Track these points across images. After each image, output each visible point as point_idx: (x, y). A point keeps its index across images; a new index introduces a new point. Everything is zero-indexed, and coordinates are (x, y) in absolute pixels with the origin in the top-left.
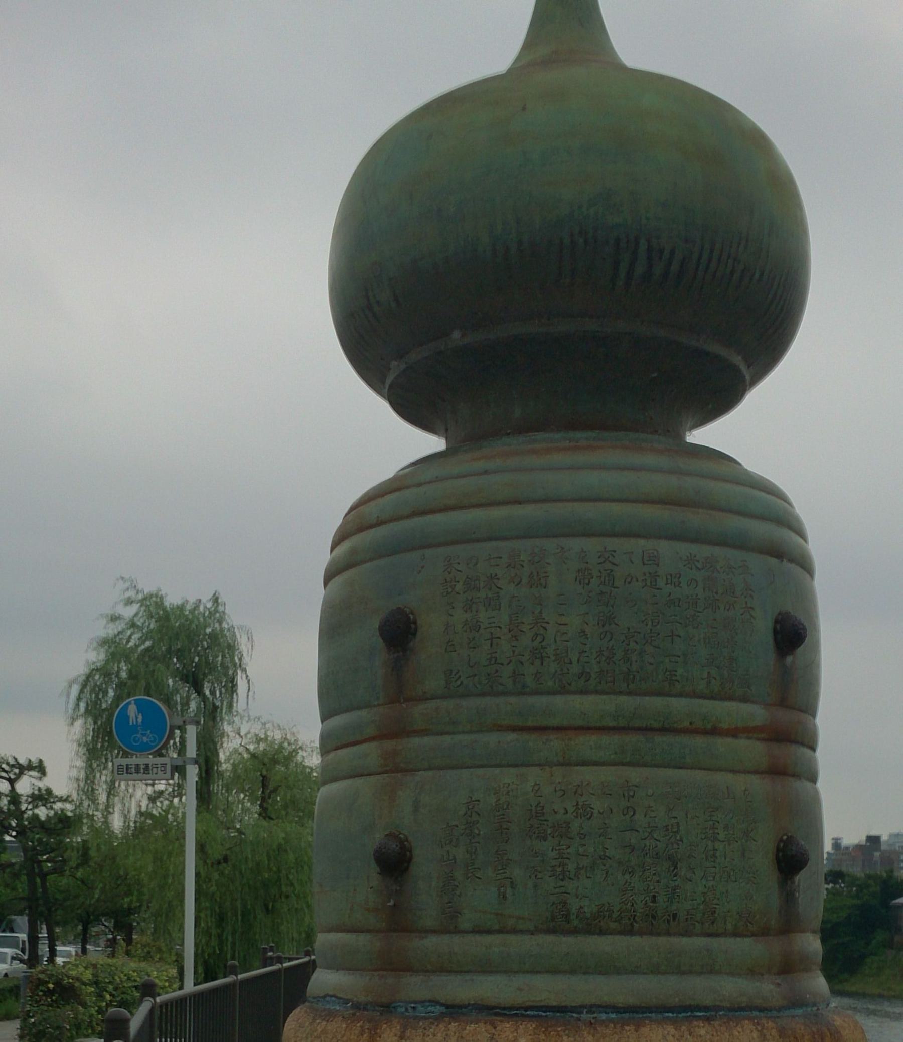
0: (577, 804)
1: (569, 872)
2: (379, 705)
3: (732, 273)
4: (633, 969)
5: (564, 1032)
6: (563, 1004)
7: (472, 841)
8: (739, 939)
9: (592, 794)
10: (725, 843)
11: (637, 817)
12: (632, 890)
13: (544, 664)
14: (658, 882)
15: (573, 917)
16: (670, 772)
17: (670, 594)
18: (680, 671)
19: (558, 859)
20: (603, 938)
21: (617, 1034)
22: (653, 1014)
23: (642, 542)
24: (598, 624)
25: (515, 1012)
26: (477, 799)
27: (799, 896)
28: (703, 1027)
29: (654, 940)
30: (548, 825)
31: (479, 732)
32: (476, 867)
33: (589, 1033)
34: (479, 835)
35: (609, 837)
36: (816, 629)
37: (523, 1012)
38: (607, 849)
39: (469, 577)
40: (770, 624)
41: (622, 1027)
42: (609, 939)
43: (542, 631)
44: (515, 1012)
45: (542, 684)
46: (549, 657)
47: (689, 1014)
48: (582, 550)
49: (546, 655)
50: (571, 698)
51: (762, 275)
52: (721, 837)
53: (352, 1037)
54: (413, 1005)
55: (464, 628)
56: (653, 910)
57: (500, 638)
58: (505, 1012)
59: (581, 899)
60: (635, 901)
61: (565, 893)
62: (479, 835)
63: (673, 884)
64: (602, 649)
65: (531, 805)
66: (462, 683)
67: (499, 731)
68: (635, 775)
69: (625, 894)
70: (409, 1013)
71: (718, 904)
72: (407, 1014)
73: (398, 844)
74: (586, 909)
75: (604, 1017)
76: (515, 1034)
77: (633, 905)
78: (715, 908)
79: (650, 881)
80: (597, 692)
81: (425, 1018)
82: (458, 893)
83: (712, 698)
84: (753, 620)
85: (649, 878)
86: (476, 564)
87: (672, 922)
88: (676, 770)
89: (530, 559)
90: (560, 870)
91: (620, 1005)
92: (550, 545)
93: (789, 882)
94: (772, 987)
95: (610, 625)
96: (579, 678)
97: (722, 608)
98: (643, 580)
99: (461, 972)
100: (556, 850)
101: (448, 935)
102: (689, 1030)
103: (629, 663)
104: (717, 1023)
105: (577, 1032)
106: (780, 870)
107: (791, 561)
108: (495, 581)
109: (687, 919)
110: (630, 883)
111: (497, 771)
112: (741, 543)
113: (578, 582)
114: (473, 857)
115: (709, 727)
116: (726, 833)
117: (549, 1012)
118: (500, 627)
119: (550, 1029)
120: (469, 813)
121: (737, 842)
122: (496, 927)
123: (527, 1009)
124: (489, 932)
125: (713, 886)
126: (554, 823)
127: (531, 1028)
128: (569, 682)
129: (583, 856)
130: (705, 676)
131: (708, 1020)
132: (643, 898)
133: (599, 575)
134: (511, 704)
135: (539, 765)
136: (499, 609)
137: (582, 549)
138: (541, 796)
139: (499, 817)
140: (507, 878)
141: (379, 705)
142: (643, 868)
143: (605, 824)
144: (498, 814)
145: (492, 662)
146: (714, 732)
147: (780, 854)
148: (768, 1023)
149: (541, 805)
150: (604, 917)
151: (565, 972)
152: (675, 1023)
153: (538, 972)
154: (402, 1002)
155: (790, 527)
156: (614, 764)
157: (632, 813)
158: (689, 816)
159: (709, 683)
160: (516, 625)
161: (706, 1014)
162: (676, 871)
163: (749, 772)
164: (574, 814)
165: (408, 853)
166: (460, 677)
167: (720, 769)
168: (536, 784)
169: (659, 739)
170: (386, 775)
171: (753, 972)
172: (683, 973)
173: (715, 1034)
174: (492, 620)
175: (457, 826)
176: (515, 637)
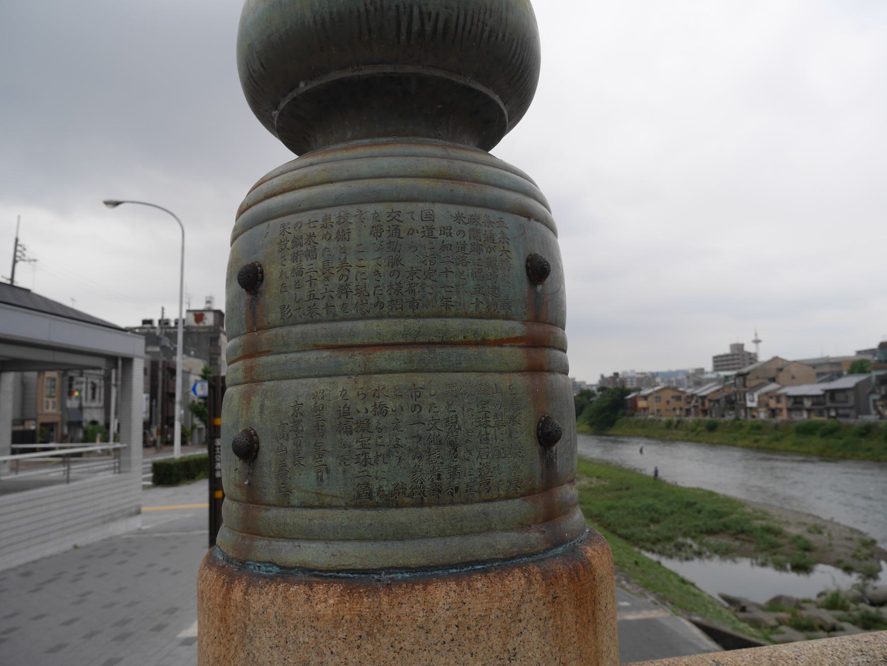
0: (375, 405)
1: (370, 459)
2: (244, 334)
3: (483, 31)
4: (424, 534)
5: (365, 593)
6: (367, 567)
7: (299, 435)
8: (510, 501)
9: (386, 396)
10: (495, 428)
11: (422, 412)
12: (421, 471)
13: (348, 297)
14: (442, 463)
15: (374, 495)
16: (448, 376)
17: (444, 241)
18: (454, 298)
19: (361, 449)
20: (399, 511)
21: (407, 593)
22: (440, 572)
23: (421, 205)
24: (388, 265)
25: (330, 574)
26: (301, 403)
27: (556, 461)
28: (480, 580)
29: (440, 510)
30: (352, 422)
31: (305, 351)
32: (301, 456)
33: (385, 594)
34: (302, 431)
35: (401, 429)
36: (559, 267)
37: (336, 574)
38: (400, 439)
39: (296, 237)
40: (523, 263)
41: (413, 586)
42: (405, 510)
43: (347, 273)
44: (330, 574)
45: (348, 312)
46: (352, 292)
47: (470, 568)
48: (376, 213)
49: (350, 290)
50: (369, 322)
51: (504, 36)
52: (492, 423)
53: (217, 588)
54: (258, 565)
55: (292, 274)
56: (438, 486)
57: (316, 279)
58: (322, 574)
59: (380, 480)
60: (423, 480)
61: (367, 476)
62: (302, 431)
63: (454, 464)
64: (392, 284)
65: (340, 407)
66: (292, 315)
67: (317, 349)
68: (420, 379)
69: (415, 475)
70: (256, 570)
71: (492, 477)
72: (255, 571)
73: (248, 438)
74: (384, 488)
75: (399, 576)
76: (326, 596)
77: (422, 483)
78: (490, 479)
79: (436, 463)
80: (390, 317)
81: (265, 577)
82: (288, 476)
83: (481, 317)
84: (509, 260)
85: (434, 460)
86: (300, 227)
87: (454, 494)
88: (454, 374)
89: (337, 220)
90: (363, 457)
91: (413, 566)
92: (353, 210)
93: (548, 452)
94: (537, 535)
95: (397, 265)
96: (375, 307)
97: (485, 250)
98: (422, 232)
99: (292, 538)
100: (359, 442)
101: (283, 509)
102: (469, 585)
103: (413, 294)
104: (491, 575)
105: (375, 592)
106: (541, 443)
107: (538, 220)
108: (313, 238)
109: (467, 490)
110: (419, 465)
111: (316, 380)
112: (498, 206)
113: (372, 235)
114: (299, 448)
115: (479, 339)
116: (496, 420)
117: (356, 574)
118: (317, 272)
119: (354, 591)
120: (295, 414)
121: (505, 426)
122: (317, 503)
123: (339, 571)
124: (312, 507)
125: (487, 462)
126: (357, 421)
127: (339, 590)
128: (368, 310)
129: (381, 445)
130: (474, 301)
131: (485, 572)
132: (430, 477)
133: (389, 229)
134: (326, 329)
135: (347, 375)
136: (316, 258)
137: (376, 211)
138: (347, 400)
139: (317, 417)
140: (323, 465)
141: (244, 334)
142: (428, 453)
143: (397, 420)
144: (316, 414)
145: (312, 298)
146: (484, 342)
147: (540, 432)
148: (534, 568)
149: (347, 406)
150: (399, 494)
151: (369, 540)
152: (458, 579)
153: (349, 540)
154: (252, 561)
155: (536, 199)
156: (405, 372)
157: (419, 410)
158: (465, 409)
159: (477, 306)
160: (328, 269)
161: (484, 566)
162: (456, 453)
163: (513, 372)
164: (373, 412)
165: (256, 445)
166: (290, 310)
167: (489, 371)
168: (343, 390)
169: (439, 350)
170: (247, 385)
171: (523, 526)
172: (465, 534)
173: (490, 586)
174: (311, 267)
175: (287, 424)
176: (327, 278)
